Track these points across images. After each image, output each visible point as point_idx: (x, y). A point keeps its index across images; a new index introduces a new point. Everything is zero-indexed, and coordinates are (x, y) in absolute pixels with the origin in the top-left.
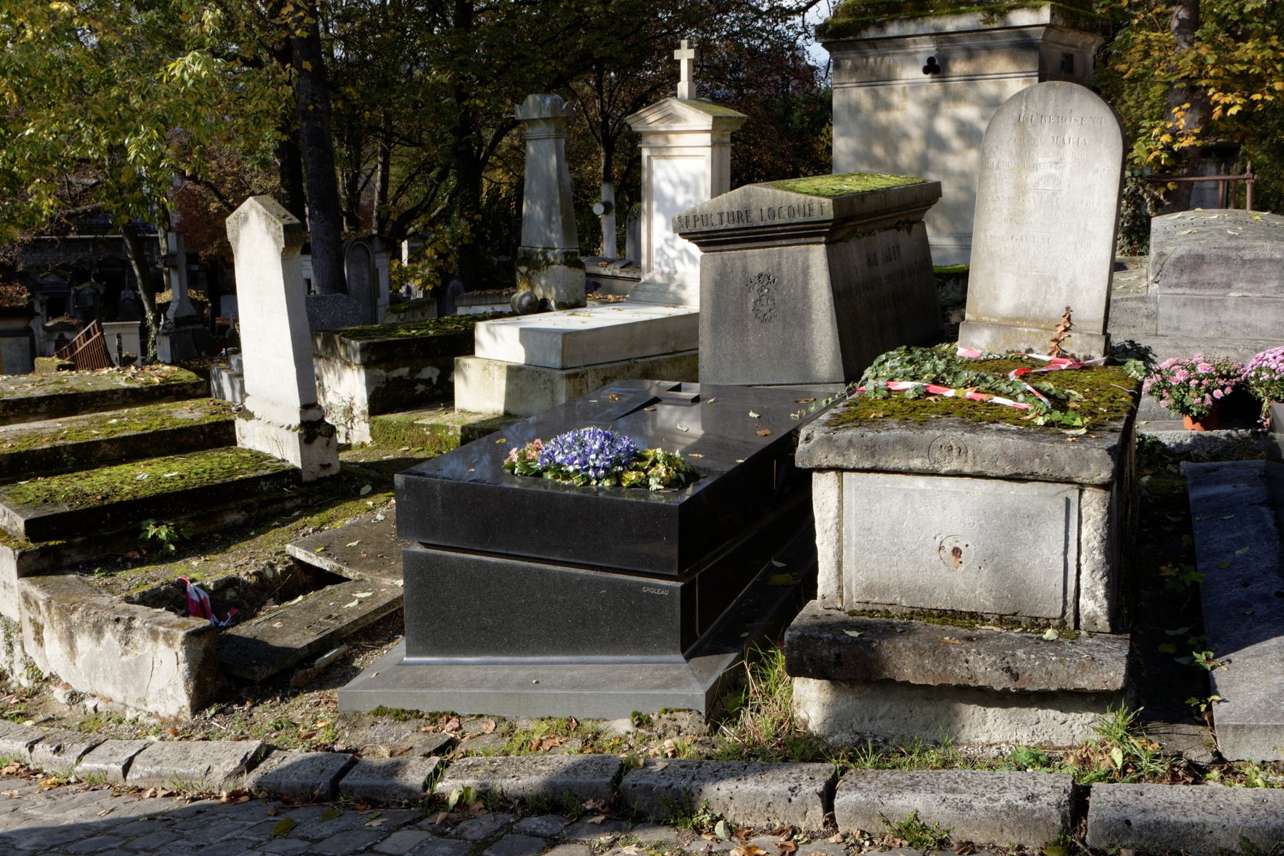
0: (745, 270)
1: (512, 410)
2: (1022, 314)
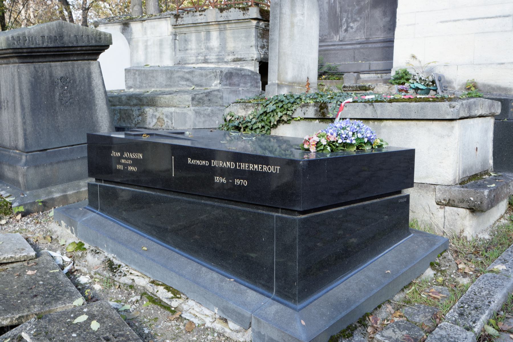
0: (51, 76)
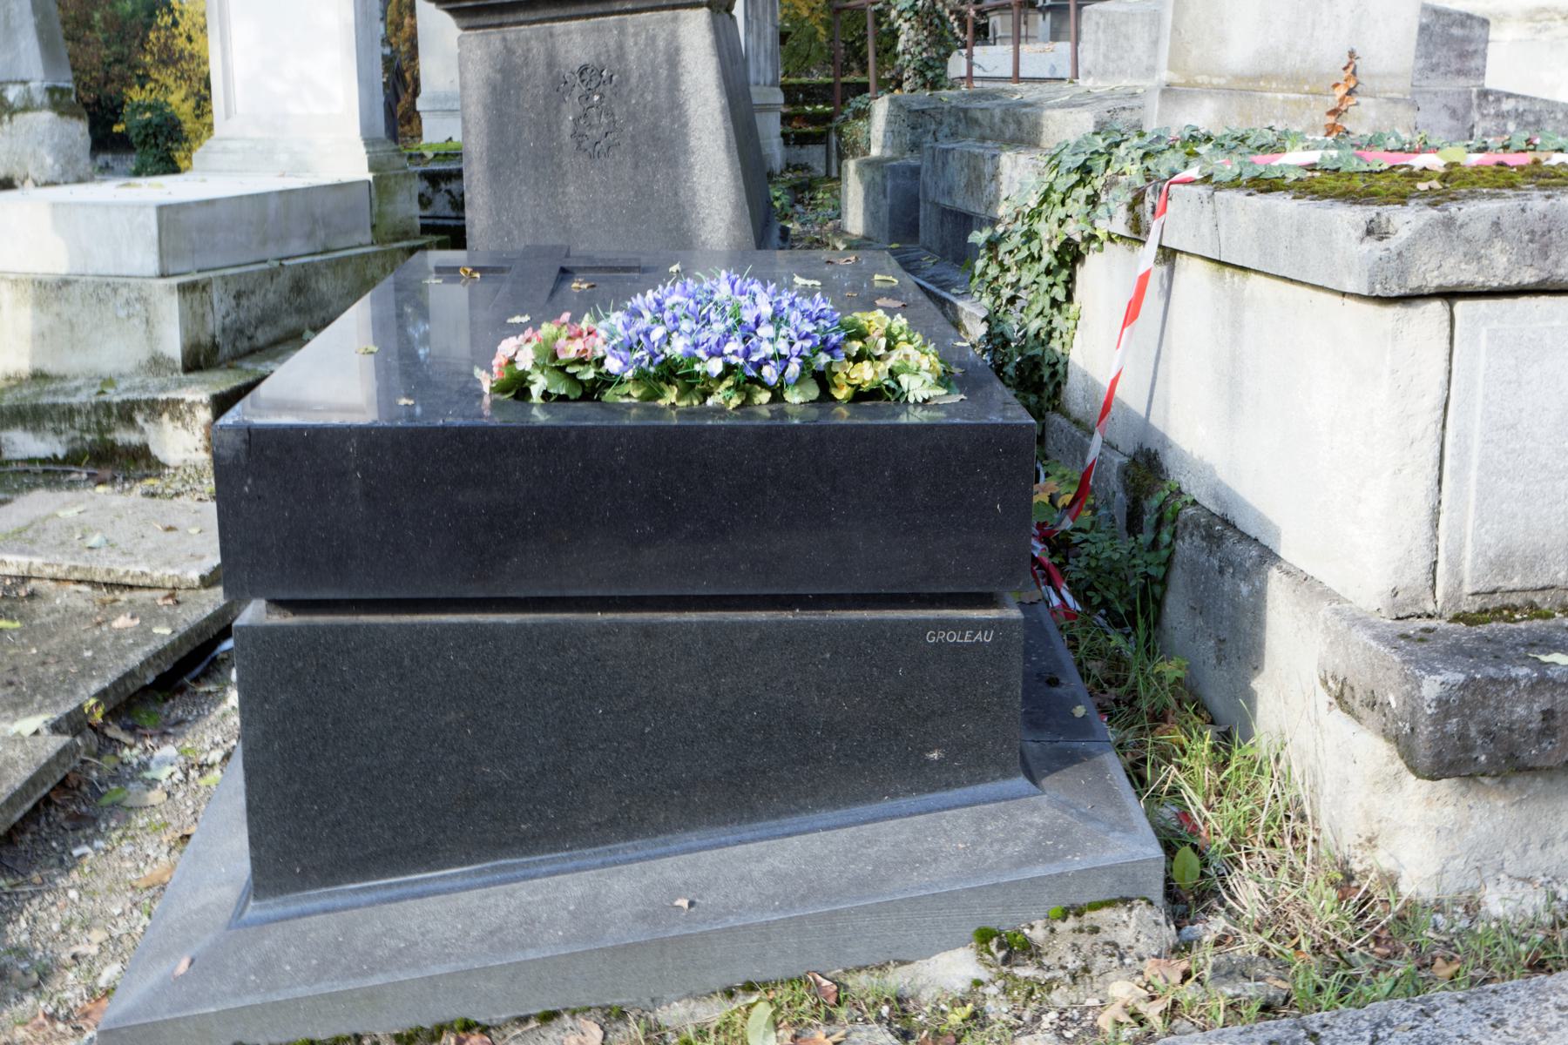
0: (551, 64)
1: (50, 367)
2: (1269, 67)
